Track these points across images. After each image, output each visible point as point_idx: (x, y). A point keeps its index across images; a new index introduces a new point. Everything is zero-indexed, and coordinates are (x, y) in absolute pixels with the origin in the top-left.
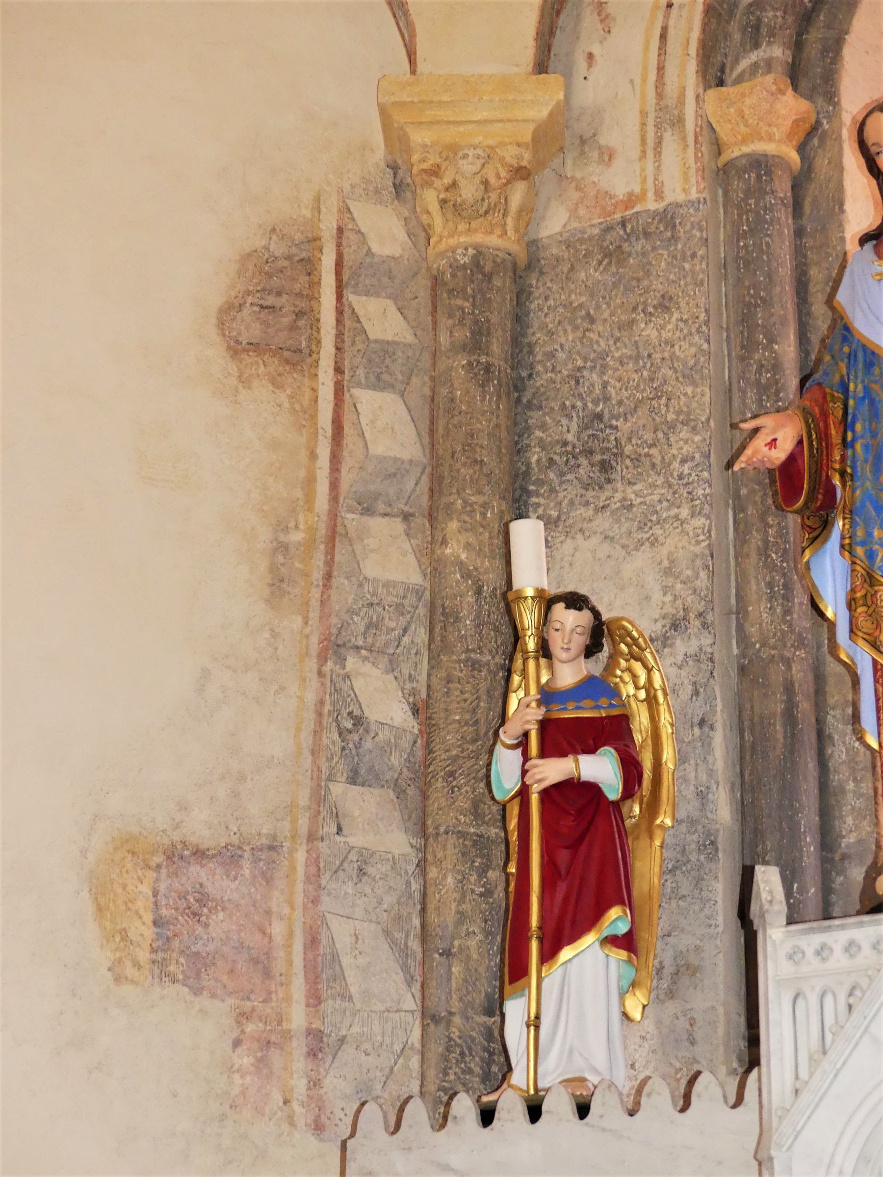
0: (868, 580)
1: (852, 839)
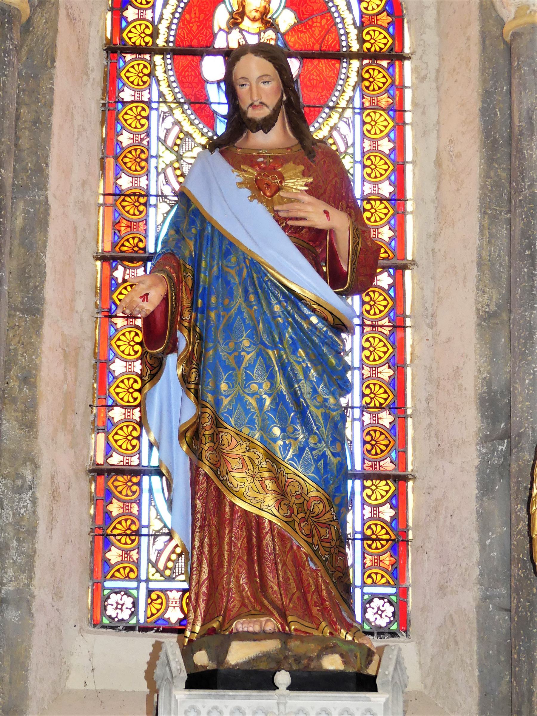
0: (215, 423)
1: (11, 587)
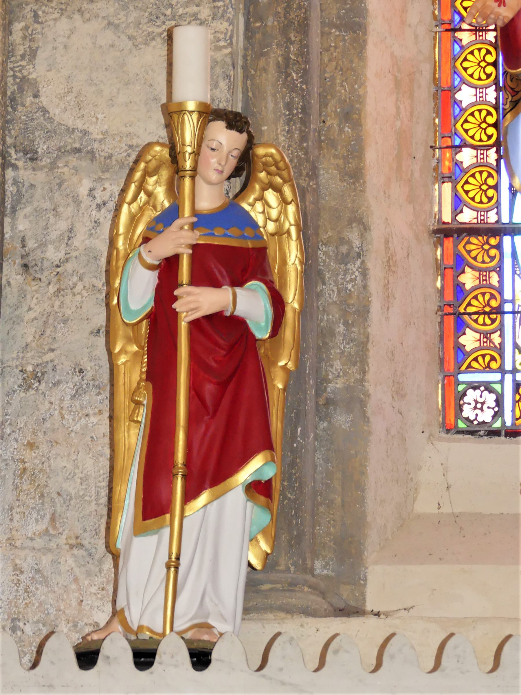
1: (339, 384)
